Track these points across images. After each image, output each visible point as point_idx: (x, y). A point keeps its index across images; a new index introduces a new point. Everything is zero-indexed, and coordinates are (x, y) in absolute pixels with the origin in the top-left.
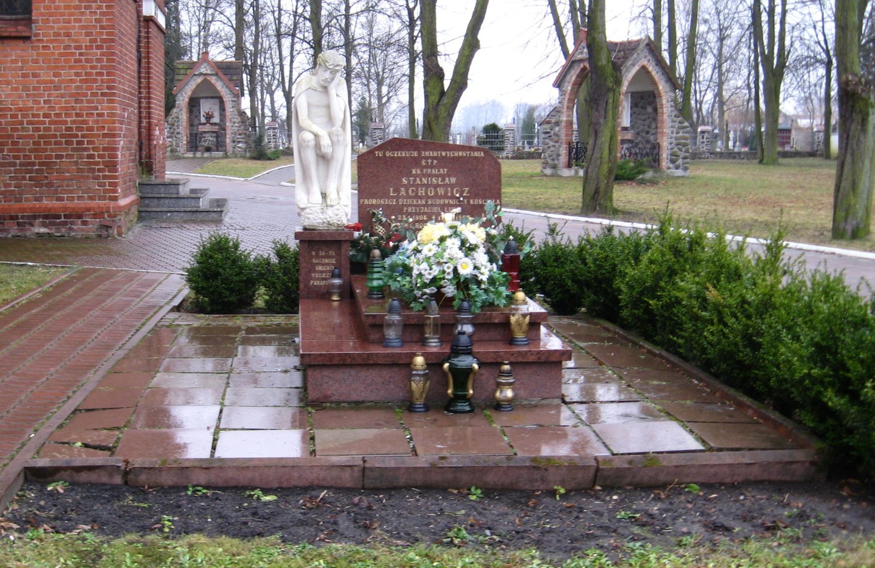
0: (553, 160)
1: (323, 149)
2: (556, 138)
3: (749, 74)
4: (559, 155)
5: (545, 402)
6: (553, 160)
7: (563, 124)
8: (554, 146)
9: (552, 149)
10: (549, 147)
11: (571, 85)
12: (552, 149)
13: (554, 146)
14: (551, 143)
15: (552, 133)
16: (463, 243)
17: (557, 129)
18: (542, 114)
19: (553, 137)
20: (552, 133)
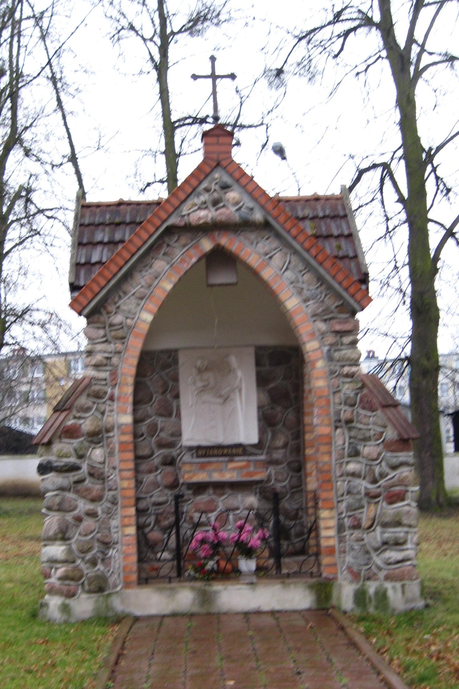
0: (93, 563)
1: (351, 230)
2: (96, 487)
3: (273, 274)
4: (107, 545)
5: (377, 56)
6: (93, 563)
7: (116, 438)
8: (92, 514)
9: (88, 523)
10: (79, 520)
11: (153, 307)
12: (88, 523)
13: (92, 514)
14: (83, 506)
15: (85, 468)
16: (53, 41)
17: (97, 454)
18: (196, 197)
19: (88, 483)
20: (85, 468)
